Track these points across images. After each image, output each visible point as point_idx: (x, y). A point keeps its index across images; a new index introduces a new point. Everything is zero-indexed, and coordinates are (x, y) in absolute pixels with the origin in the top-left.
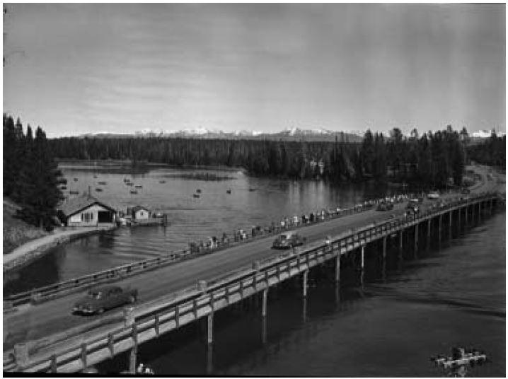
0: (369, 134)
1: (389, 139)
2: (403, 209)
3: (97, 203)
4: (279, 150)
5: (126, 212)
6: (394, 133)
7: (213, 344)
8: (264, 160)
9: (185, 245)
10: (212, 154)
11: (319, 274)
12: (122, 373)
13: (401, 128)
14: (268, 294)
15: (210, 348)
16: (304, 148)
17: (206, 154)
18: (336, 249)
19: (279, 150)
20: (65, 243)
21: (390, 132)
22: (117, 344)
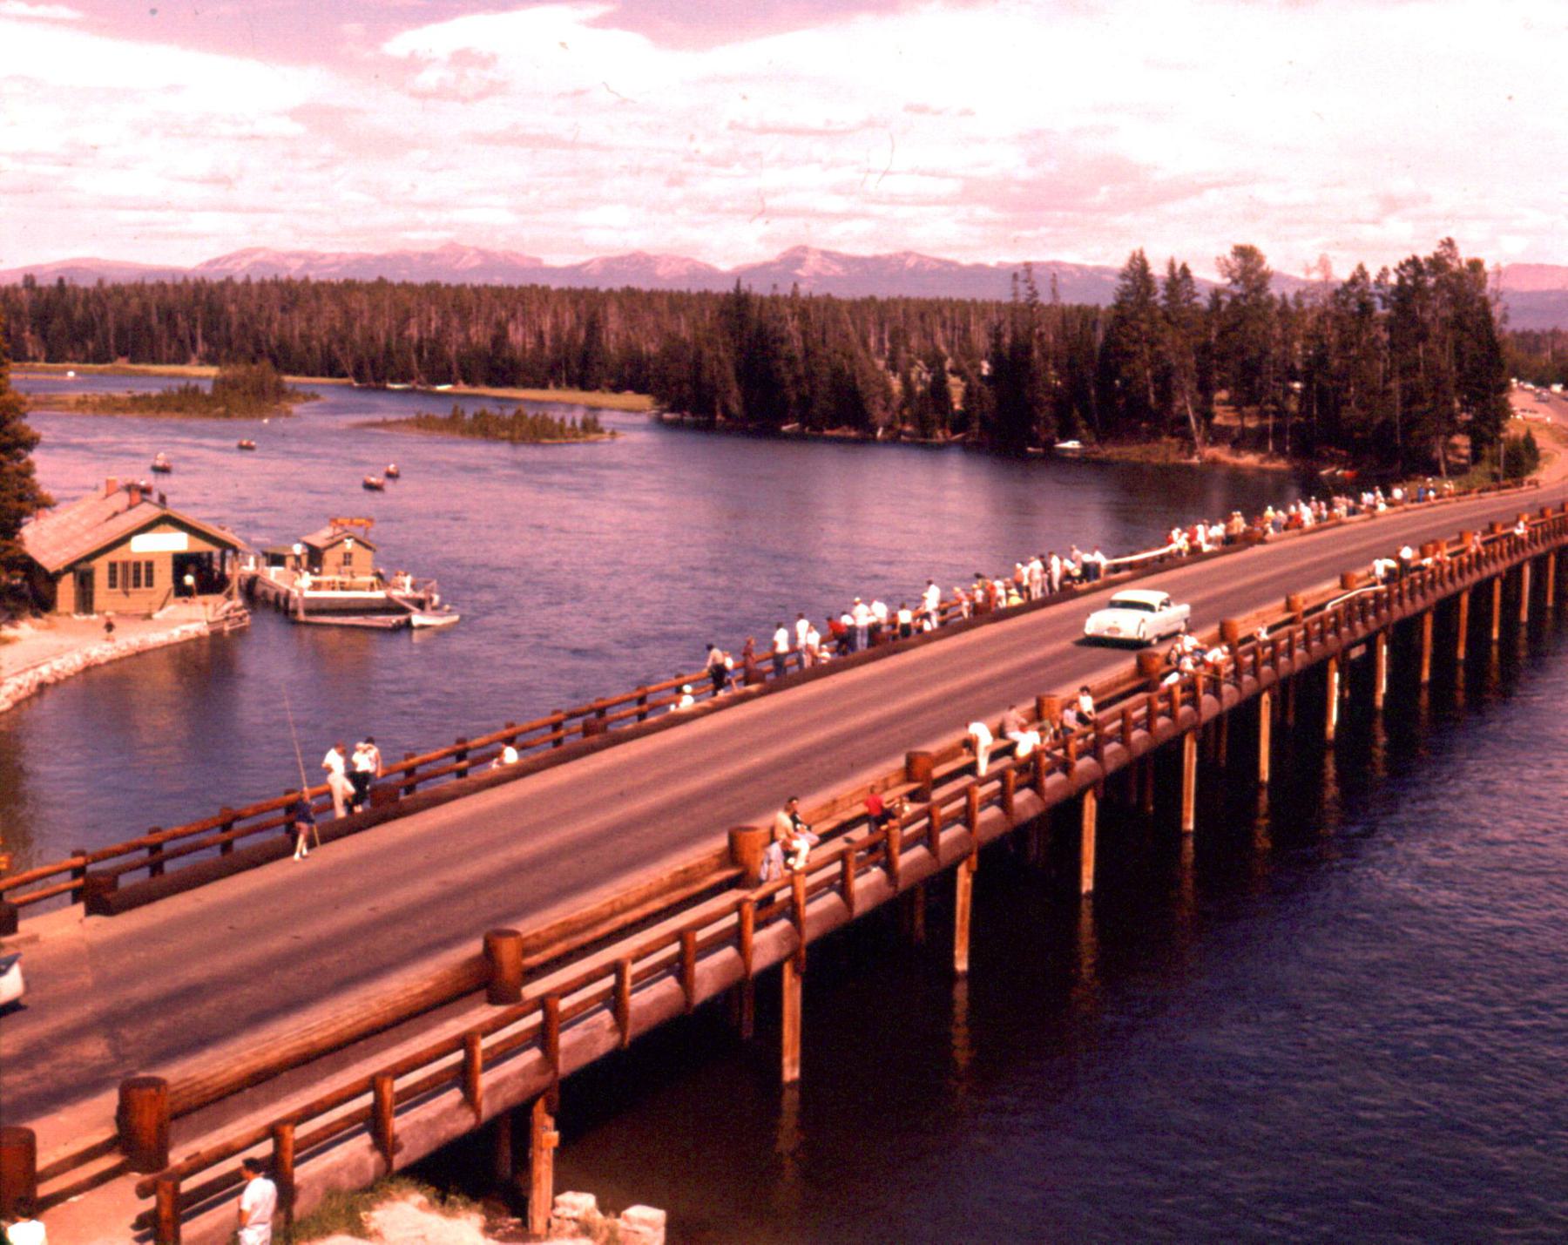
0: (1138, 270)
1: (1216, 294)
2: (1176, 608)
3: (168, 521)
4: (792, 326)
5: (1077, 572)
6: (1235, 263)
7: (971, 974)
8: (722, 362)
9: (167, 751)
10: (517, 336)
11: (868, 960)
12: (748, 1033)
13: (1262, 245)
14: (978, 878)
15: (790, 1099)
16: (844, 309)
17: (500, 339)
18: (1110, 739)
19: (792, 326)
20: (28, 699)
21: (1223, 265)
22: (635, 996)
